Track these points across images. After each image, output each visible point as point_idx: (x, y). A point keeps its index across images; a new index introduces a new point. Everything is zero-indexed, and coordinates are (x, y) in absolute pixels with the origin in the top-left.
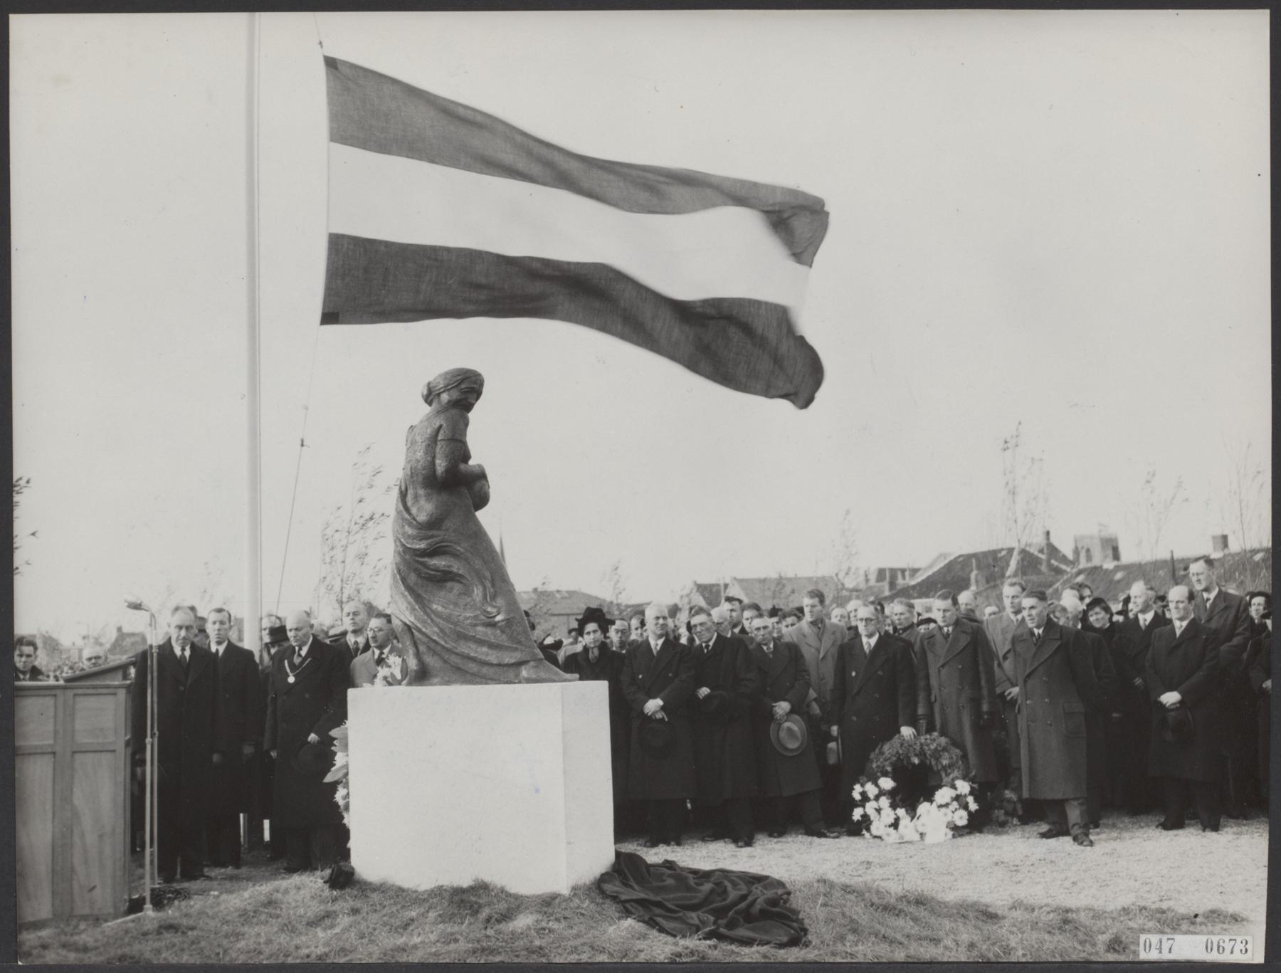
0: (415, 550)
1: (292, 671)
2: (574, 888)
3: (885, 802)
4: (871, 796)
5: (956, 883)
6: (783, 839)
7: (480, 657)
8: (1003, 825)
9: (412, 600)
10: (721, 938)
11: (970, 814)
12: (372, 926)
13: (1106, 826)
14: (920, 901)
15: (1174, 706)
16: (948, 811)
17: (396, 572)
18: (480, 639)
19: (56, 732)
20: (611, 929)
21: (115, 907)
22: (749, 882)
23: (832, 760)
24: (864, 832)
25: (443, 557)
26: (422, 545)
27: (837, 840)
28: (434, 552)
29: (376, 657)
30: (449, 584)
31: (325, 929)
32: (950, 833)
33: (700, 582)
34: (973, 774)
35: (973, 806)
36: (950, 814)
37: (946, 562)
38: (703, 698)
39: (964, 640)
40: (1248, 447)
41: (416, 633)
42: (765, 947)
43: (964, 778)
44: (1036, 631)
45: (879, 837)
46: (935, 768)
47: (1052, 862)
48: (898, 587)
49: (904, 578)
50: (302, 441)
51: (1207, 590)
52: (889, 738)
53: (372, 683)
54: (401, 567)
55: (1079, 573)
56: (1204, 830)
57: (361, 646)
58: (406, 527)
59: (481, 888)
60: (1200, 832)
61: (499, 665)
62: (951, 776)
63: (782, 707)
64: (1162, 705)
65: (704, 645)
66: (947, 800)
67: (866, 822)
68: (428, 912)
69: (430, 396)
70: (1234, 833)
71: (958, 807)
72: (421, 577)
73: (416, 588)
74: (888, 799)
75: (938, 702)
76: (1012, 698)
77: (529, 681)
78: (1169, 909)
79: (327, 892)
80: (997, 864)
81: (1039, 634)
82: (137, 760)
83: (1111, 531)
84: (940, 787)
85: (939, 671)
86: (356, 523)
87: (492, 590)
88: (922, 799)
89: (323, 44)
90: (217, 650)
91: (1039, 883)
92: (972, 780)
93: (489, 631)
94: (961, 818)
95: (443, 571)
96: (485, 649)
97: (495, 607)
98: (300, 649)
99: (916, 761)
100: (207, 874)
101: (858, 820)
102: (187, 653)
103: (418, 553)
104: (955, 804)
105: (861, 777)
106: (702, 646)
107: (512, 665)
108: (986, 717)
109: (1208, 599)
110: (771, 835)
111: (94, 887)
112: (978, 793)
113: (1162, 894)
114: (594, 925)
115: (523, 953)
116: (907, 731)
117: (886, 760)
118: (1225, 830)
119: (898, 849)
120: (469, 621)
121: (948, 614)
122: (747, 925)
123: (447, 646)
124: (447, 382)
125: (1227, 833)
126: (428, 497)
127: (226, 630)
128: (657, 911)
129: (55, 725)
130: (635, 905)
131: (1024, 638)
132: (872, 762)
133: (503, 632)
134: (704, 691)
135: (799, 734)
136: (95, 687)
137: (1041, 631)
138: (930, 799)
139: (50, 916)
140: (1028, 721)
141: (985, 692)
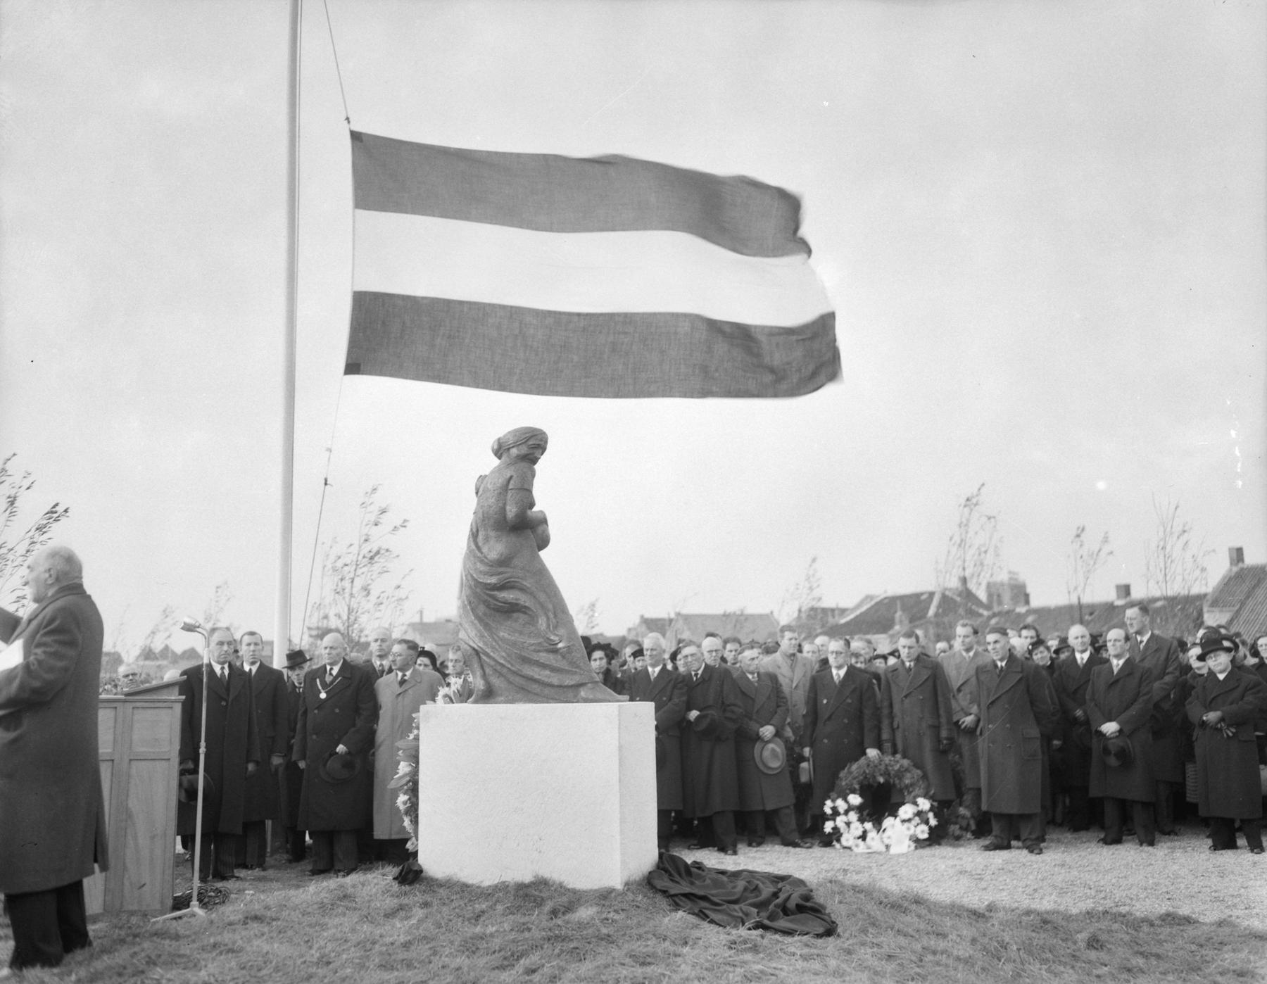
0: (486, 584)
1: (323, 689)
2: (627, 884)
3: (853, 816)
4: (841, 810)
6: (762, 848)
7: (543, 679)
8: (958, 838)
10: (766, 928)
11: (930, 828)
12: (446, 917)
13: (1052, 841)
14: (918, 901)
15: (1115, 735)
17: (466, 603)
18: (543, 663)
19: (115, 741)
20: (667, 919)
21: (162, 903)
22: (774, 881)
23: (804, 778)
24: (835, 843)
25: (511, 591)
26: (493, 580)
27: (811, 850)
28: (502, 587)
29: (399, 678)
30: (515, 615)
31: (402, 920)
32: (913, 845)
33: (647, 615)
34: (932, 792)
35: (933, 822)
36: (913, 828)
37: (873, 603)
39: (925, 674)
40: (1176, 508)
41: (484, 657)
42: (805, 937)
43: (925, 796)
44: (999, 664)
45: (849, 848)
46: (899, 786)
47: (1010, 871)
48: (829, 625)
49: (834, 617)
50: (326, 480)
51: (1139, 632)
52: (857, 760)
53: (434, 701)
54: (472, 598)
55: (994, 615)
56: (1141, 845)
57: (386, 668)
58: (478, 564)
59: (541, 883)
60: (1138, 846)
61: (560, 686)
62: (913, 794)
63: (767, 731)
64: (1101, 734)
65: (693, 673)
67: (836, 834)
68: (495, 905)
69: (500, 450)
70: (1168, 848)
71: (919, 822)
72: (490, 608)
75: (900, 730)
76: (966, 727)
77: (586, 701)
78: (1128, 913)
79: (396, 887)
80: (961, 873)
81: (1002, 667)
82: (188, 771)
83: (408, 528)
84: (903, 804)
85: (902, 701)
86: (364, 557)
87: (554, 621)
88: (887, 814)
89: (351, 120)
90: (250, 670)
91: (1003, 889)
92: (932, 798)
93: (551, 656)
94: (923, 832)
95: (510, 603)
96: (547, 672)
97: (557, 635)
98: (331, 669)
99: (882, 780)
100: (237, 875)
101: (829, 833)
102: (226, 672)
103: (489, 587)
104: (917, 820)
105: (831, 794)
106: (691, 674)
107: (572, 686)
108: (945, 742)
109: (1141, 642)
110: (750, 845)
112: (936, 810)
113: (1116, 900)
114: (650, 916)
115: (593, 940)
116: (872, 753)
117: (854, 779)
118: (1160, 844)
119: (869, 858)
120: (533, 647)
121: (912, 650)
122: (786, 918)
123: (513, 669)
124: (516, 439)
125: (1162, 847)
126: (498, 539)
127: (259, 650)
128: (704, 904)
129: (115, 734)
130: (684, 899)
131: (988, 669)
132: (841, 780)
133: (564, 657)
134: (694, 714)
135: (781, 757)
136: (153, 701)
137: (1004, 664)
139: (101, 911)
140: (989, 743)
141: (943, 720)
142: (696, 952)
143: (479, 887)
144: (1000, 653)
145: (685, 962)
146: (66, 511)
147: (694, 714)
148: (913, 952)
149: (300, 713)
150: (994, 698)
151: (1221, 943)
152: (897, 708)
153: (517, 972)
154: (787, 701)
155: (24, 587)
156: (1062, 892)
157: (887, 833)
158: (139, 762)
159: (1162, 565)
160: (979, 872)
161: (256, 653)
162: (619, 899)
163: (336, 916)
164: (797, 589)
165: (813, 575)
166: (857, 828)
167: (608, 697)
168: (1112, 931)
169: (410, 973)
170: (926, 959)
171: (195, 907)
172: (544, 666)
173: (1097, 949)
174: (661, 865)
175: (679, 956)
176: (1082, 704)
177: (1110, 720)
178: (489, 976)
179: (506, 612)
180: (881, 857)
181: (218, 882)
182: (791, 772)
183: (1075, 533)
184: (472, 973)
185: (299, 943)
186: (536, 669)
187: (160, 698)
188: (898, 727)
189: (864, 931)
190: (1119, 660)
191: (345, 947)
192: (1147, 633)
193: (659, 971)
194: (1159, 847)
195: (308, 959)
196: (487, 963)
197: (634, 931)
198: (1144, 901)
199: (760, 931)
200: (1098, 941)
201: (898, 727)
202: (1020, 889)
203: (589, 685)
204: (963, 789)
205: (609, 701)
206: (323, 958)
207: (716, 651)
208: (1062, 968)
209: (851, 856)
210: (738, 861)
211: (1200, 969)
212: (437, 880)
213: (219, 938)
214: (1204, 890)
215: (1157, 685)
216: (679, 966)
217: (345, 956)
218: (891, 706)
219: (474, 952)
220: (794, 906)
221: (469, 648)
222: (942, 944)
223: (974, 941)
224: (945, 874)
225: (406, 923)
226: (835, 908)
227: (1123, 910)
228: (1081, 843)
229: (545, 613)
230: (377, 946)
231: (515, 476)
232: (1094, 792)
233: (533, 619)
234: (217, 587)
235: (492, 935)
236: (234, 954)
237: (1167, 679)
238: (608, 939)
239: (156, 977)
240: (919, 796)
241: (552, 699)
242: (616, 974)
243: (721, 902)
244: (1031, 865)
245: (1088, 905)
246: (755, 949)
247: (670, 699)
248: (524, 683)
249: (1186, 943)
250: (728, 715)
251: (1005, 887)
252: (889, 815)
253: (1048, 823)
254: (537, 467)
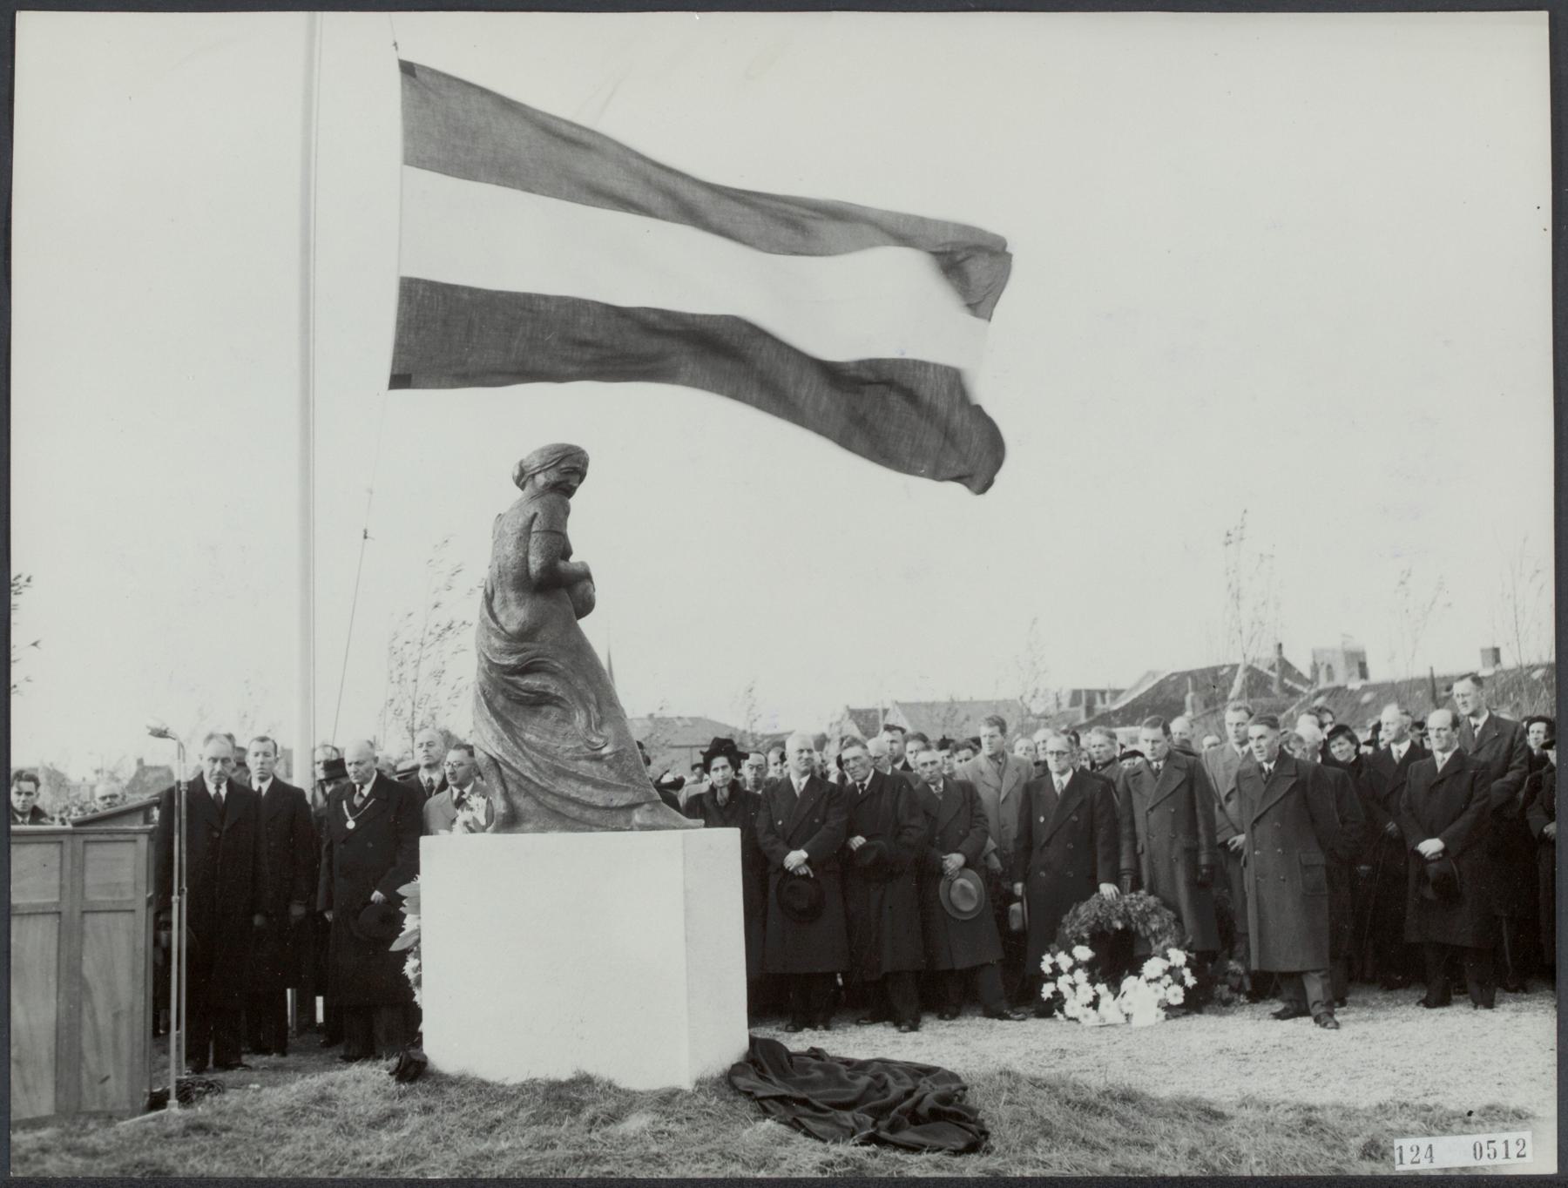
0: (503, 666)
1: (351, 815)
2: (699, 1083)
3: (1081, 976)
4: (1064, 968)
5: (1171, 1076)
7: (582, 798)
8: (1227, 1003)
9: (499, 728)
10: (882, 1143)
11: (1186, 990)
12: (448, 1128)
13: (1355, 1004)
14: (1128, 1098)
16: (1159, 986)
17: (479, 693)
18: (582, 776)
19: (61, 887)
20: (746, 1133)
21: (132, 1102)
23: (1016, 925)
24: (1057, 1013)
25: (538, 675)
26: (512, 661)
27: (1023, 1023)
28: (526, 669)
29: (455, 797)
30: (545, 709)
31: (390, 1132)
32: (1163, 1014)
33: (853, 707)
34: (1189, 940)
35: (1190, 981)
37: (1155, 681)
38: (858, 849)
39: (1178, 777)
41: (504, 769)
42: (937, 1154)
43: (1179, 946)
44: (1266, 766)
45: (1075, 1019)
47: (1289, 1048)
48: (1097, 713)
50: (366, 532)
51: (1474, 714)
54: (486, 687)
55: (1319, 694)
56: (1476, 1007)
57: (436, 784)
60: (1471, 1009)
61: (606, 808)
62: (1163, 944)
63: (955, 860)
64: (1419, 855)
65: (858, 784)
67: (1058, 1000)
68: (518, 1111)
70: (1513, 1010)
71: (1171, 981)
72: (510, 699)
73: (504, 713)
74: (1084, 972)
75: (1146, 853)
77: (643, 828)
79: (393, 1086)
80: (1221, 1052)
81: (1269, 770)
85: (1147, 815)
86: (430, 634)
87: (598, 716)
88: (1127, 972)
90: (260, 788)
92: (1189, 949)
93: (594, 766)
94: (1176, 996)
95: (536, 692)
96: (589, 789)
97: (601, 737)
98: (362, 787)
99: (1119, 925)
101: (1049, 999)
102: (223, 792)
104: (1168, 978)
107: (622, 808)
108: (1204, 871)
109: (1476, 726)
110: (941, 1017)
111: (107, 1078)
112: (1195, 964)
114: (724, 1127)
115: (636, 1161)
116: (1107, 889)
118: (1502, 1006)
119: (1099, 1033)
121: (1158, 746)
122: (913, 1127)
123: (542, 784)
124: (543, 460)
125: (1504, 1010)
126: (520, 603)
127: (270, 763)
130: (775, 1103)
131: (1251, 774)
132: (1065, 927)
133: (611, 767)
134: (858, 841)
136: (110, 833)
137: (1272, 766)
138: (1137, 972)
139: (53, 1113)
141: (1203, 841)
143: (503, 1086)
146: (28, 580)
147: (858, 841)
149: (324, 846)
152: (1140, 828)
160: (1245, 1051)
162: (687, 1102)
166: (1086, 992)
167: (673, 823)
173: (1376, 1159)
179: (532, 705)
180: (1116, 1032)
181: (220, 1072)
188: (1143, 852)
192: (1484, 714)
194: (1500, 1010)
199: (872, 1148)
201: (1143, 852)
203: (647, 806)
209: (1076, 1030)
210: (920, 1040)
221: (485, 756)
227: (1430, 1102)
228: (1394, 1007)
235: (502, 1154)
237: (1510, 776)
243: (827, 1108)
245: (1384, 1095)
248: (557, 803)
251: (1278, 1071)
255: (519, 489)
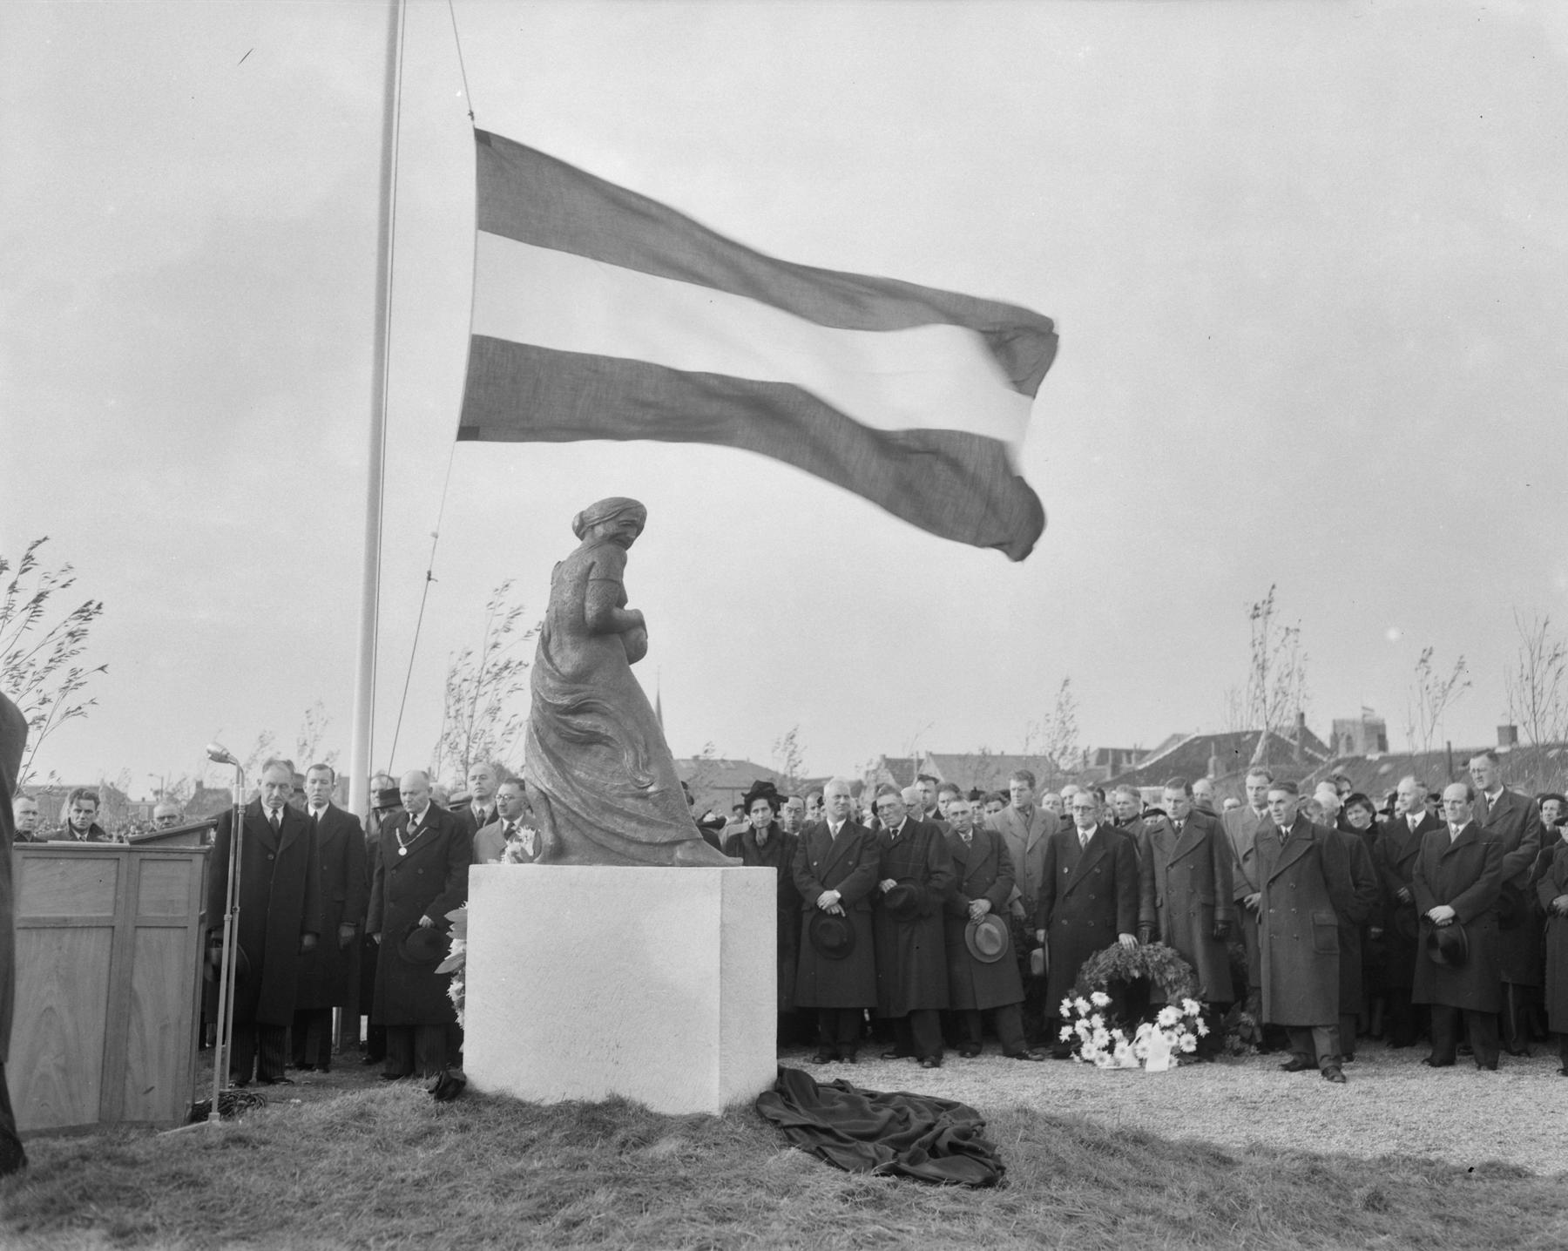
1: (403, 843)
2: (728, 1110)
3: (1098, 1021)
4: (1082, 1013)
8: (1238, 1053)
9: (551, 764)
10: (901, 1174)
11: (1199, 1038)
13: (1362, 1059)
14: (1140, 1139)
17: (532, 730)
18: (628, 813)
20: (771, 1160)
21: (175, 1113)
23: (1037, 969)
24: (1073, 1055)
25: (588, 716)
26: (566, 701)
27: (1041, 1063)
28: (578, 709)
29: (505, 828)
30: (595, 748)
31: (425, 1149)
33: (888, 756)
35: (1203, 1030)
36: (1175, 1038)
38: (889, 891)
39: (1198, 836)
40: (1545, 625)
41: (553, 803)
42: (955, 1187)
43: (1193, 997)
44: (1283, 829)
45: (1091, 1062)
46: (1159, 984)
47: (1297, 1099)
48: (1123, 772)
49: (1129, 761)
50: (429, 573)
51: (1489, 789)
52: (1106, 947)
55: (1338, 763)
56: (1479, 1068)
57: (488, 815)
60: (1475, 1070)
62: (1178, 993)
66: (1172, 1021)
67: (1075, 1043)
68: (552, 1131)
74: (1101, 1017)
76: (1252, 906)
79: (432, 1103)
81: (1287, 833)
82: (212, 939)
84: (1165, 1006)
86: (488, 672)
87: (645, 756)
89: (475, 115)
92: (1202, 1000)
93: (640, 803)
94: (1189, 1043)
95: (587, 732)
96: (633, 825)
97: (647, 776)
99: (1137, 974)
101: (1066, 1041)
102: (280, 816)
107: (665, 844)
109: (1491, 800)
110: (963, 1055)
116: (1126, 939)
119: (1113, 1076)
120: (617, 791)
121: (1180, 805)
122: (933, 1160)
123: (589, 819)
124: (603, 513)
125: (1507, 1072)
126: (575, 646)
127: (327, 790)
128: (825, 1139)
130: (801, 1132)
131: (1270, 836)
132: (1084, 973)
133: (655, 805)
134: (889, 884)
135: (1000, 940)
136: (166, 851)
137: (1289, 829)
138: (1152, 1019)
139: (96, 1121)
141: (1220, 897)
142: (797, 1204)
144: (1284, 816)
145: (779, 1220)
146: (99, 607)
147: (889, 884)
148: (1105, 1210)
149: (376, 871)
150: (1275, 874)
151: (1555, 1206)
153: (554, 1225)
154: (1013, 869)
155: (41, 706)
156: (1359, 1130)
157: (1142, 1044)
158: (148, 930)
159: (1530, 701)
161: (321, 793)
163: (344, 1140)
164: (1048, 721)
165: (1067, 702)
166: (1102, 1036)
167: (713, 860)
168: (1409, 1185)
169: (413, 1222)
170: (1124, 1222)
171: (215, 1115)
172: (630, 817)
174: (779, 1084)
175: (773, 1210)
176: (1407, 880)
177: (1443, 904)
178: (514, 1229)
179: (582, 744)
182: (1020, 961)
183: (1420, 656)
184: (494, 1225)
185: (283, 1177)
186: (619, 820)
187: (176, 847)
188: (1161, 906)
189: (1046, 1180)
190: (484, 804)
191: (340, 1184)
192: (1500, 788)
193: (739, 1230)
194: (1502, 1072)
195: (289, 1199)
196: (517, 1211)
197: (723, 1174)
198: (1467, 1144)
199: (892, 1179)
200: (1381, 1199)
202: (1305, 1124)
203: (688, 843)
204: (1248, 988)
205: (714, 865)
206: (307, 1196)
207: (281, 786)
208: (1321, 1236)
209: (1092, 1072)
211: (1517, 1241)
212: (485, 1095)
213: (183, 1166)
214: (1550, 1132)
215: (1508, 857)
216: (769, 1225)
217: (336, 1196)
218: (1153, 878)
219: (505, 1195)
220: (946, 1144)
221: (535, 790)
222: (1152, 1200)
223: (1202, 1196)
224: (1209, 1100)
225: (431, 1152)
226: (1012, 1150)
227: (1433, 1156)
229: (633, 746)
230: (380, 1183)
231: (598, 563)
232: (1419, 997)
233: (615, 758)
234: (307, 712)
235: (535, 1173)
236: (198, 1189)
238: (685, 1184)
239: (88, 1215)
240: (1185, 996)
241: (640, 860)
242: (680, 1234)
243: (846, 1137)
244: (1326, 1092)
245: (1386, 1148)
246: (879, 1202)
247: (858, 864)
248: (603, 837)
249: (1506, 1204)
250: (934, 883)
252: (1145, 1022)
253: (1359, 1036)
254: (629, 552)
255: (579, 540)
